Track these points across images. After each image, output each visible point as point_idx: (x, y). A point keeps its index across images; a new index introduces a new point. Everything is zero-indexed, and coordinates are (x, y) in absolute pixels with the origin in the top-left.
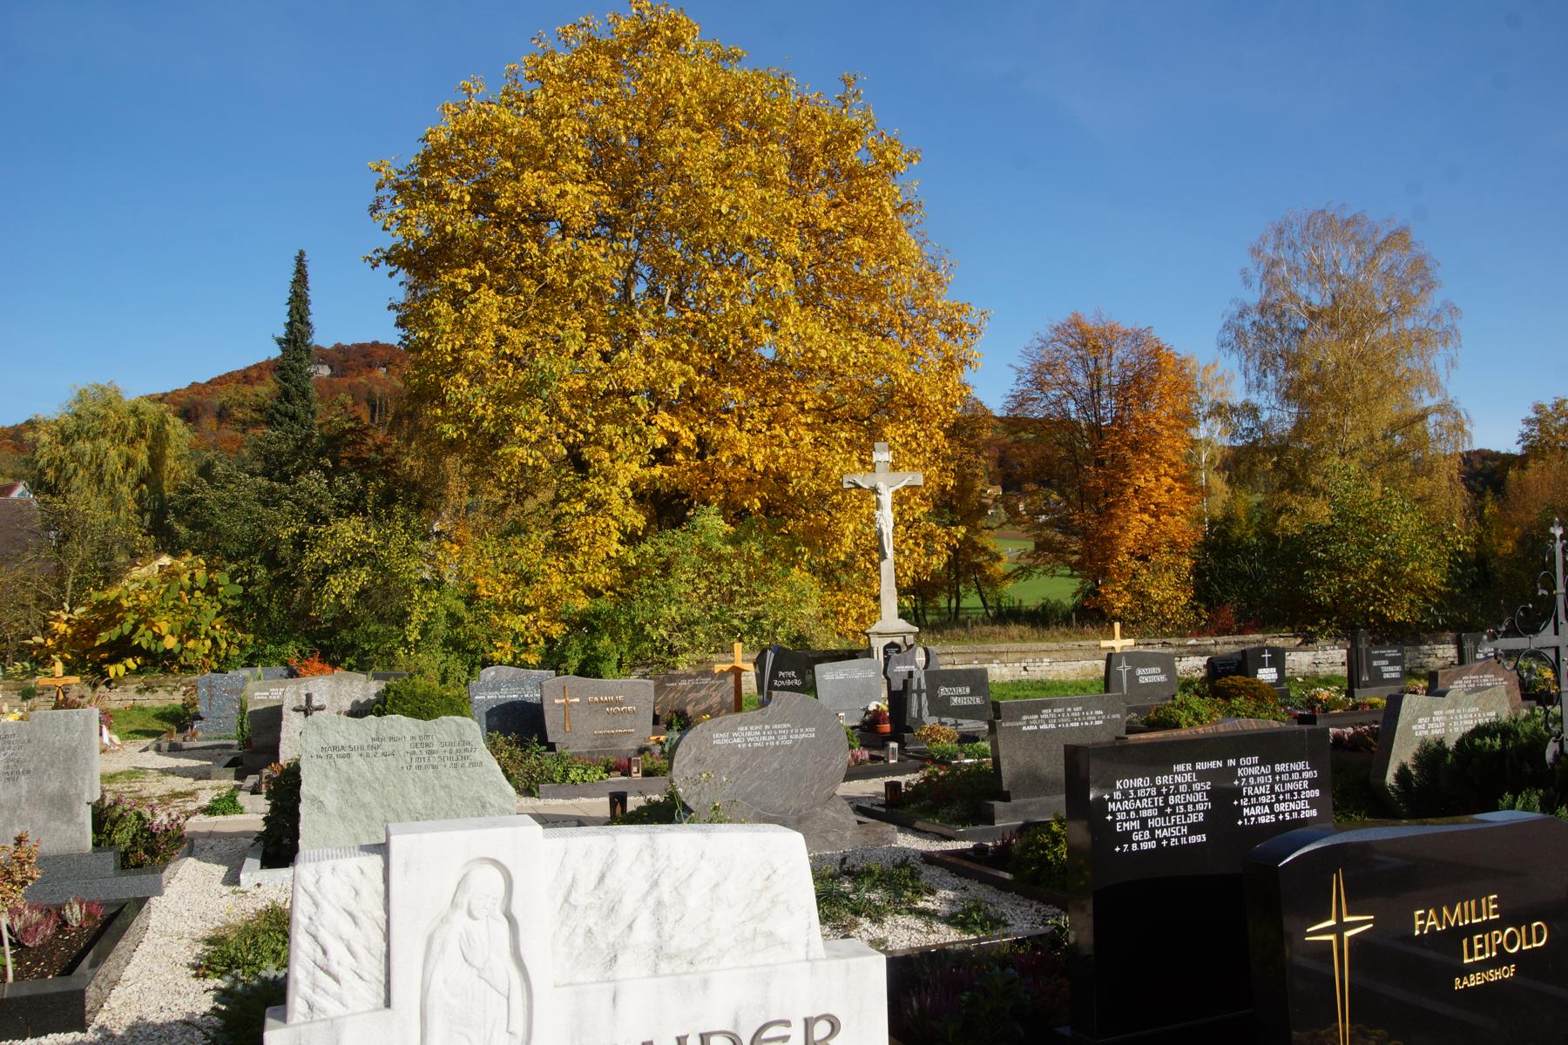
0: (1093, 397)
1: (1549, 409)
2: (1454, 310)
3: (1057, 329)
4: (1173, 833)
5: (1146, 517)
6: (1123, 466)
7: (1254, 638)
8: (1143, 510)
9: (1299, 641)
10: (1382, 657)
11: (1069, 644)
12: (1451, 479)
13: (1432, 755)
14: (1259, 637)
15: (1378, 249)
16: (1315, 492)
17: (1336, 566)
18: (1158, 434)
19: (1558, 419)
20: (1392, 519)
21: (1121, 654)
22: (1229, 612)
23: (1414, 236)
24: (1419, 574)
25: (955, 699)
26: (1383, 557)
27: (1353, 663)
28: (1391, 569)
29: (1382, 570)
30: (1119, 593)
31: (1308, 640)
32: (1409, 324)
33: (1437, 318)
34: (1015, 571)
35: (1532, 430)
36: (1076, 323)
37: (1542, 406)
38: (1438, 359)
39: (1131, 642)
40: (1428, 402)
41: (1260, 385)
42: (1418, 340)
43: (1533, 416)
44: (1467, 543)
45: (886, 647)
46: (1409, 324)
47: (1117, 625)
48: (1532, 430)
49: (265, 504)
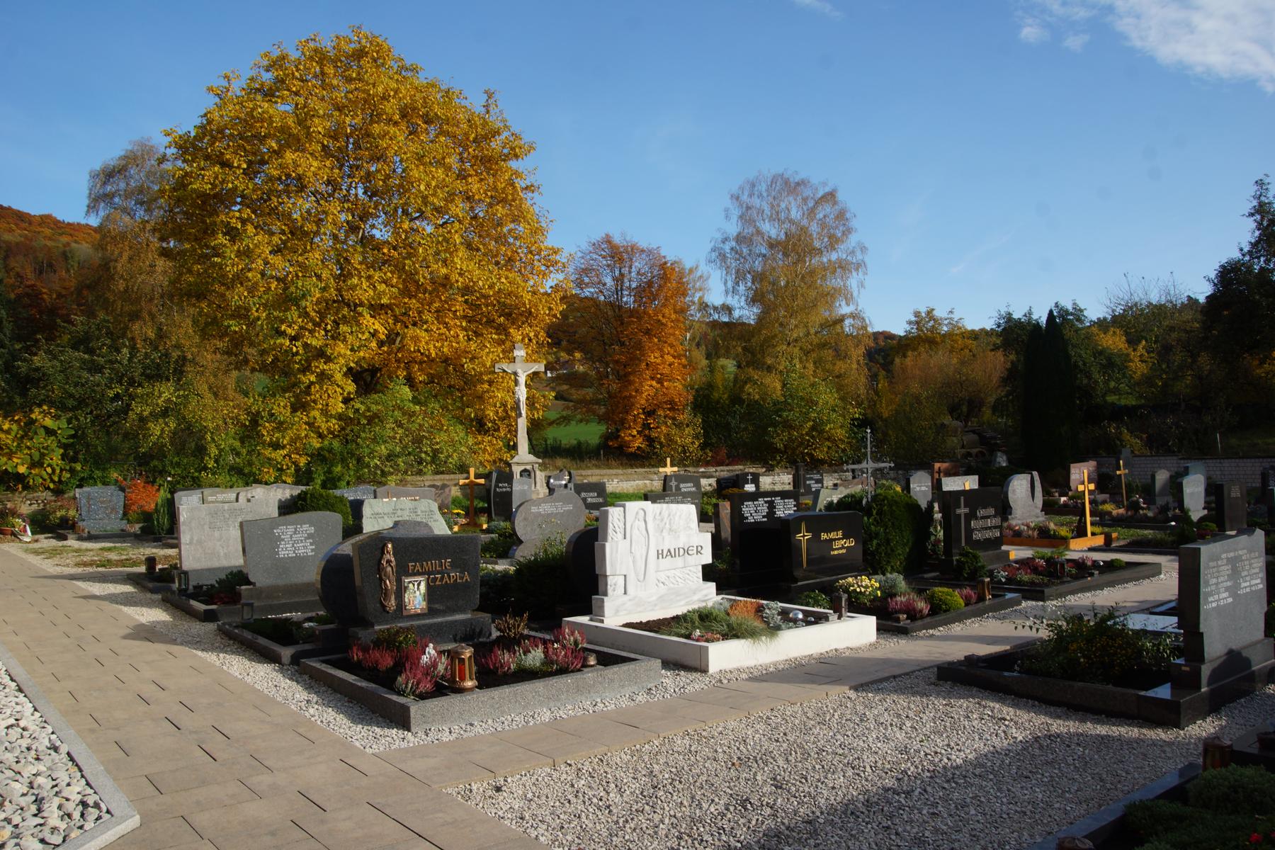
0: (617, 294)
1: (923, 315)
2: (864, 249)
3: (594, 244)
4: (759, 518)
5: (654, 383)
6: (639, 345)
7: (738, 468)
8: (652, 379)
9: (764, 470)
10: (811, 479)
11: (630, 471)
12: (858, 362)
13: (830, 506)
14: (741, 467)
15: (817, 203)
16: (769, 369)
17: (788, 425)
18: (662, 324)
19: (929, 322)
20: (819, 398)
21: (671, 476)
22: (724, 451)
23: (840, 196)
24: (833, 431)
25: (589, 499)
26: (813, 421)
27: (796, 482)
28: (817, 428)
29: (813, 428)
30: (634, 436)
31: (770, 469)
32: (834, 256)
33: (853, 252)
34: (558, 419)
35: (912, 328)
36: (608, 240)
37: (919, 312)
38: (853, 282)
39: (675, 469)
40: (845, 309)
41: (734, 291)
42: (840, 267)
43: (913, 319)
44: (860, 414)
45: (521, 472)
46: (834, 256)
47: (668, 460)
48: (912, 328)
49: (89, 371)
